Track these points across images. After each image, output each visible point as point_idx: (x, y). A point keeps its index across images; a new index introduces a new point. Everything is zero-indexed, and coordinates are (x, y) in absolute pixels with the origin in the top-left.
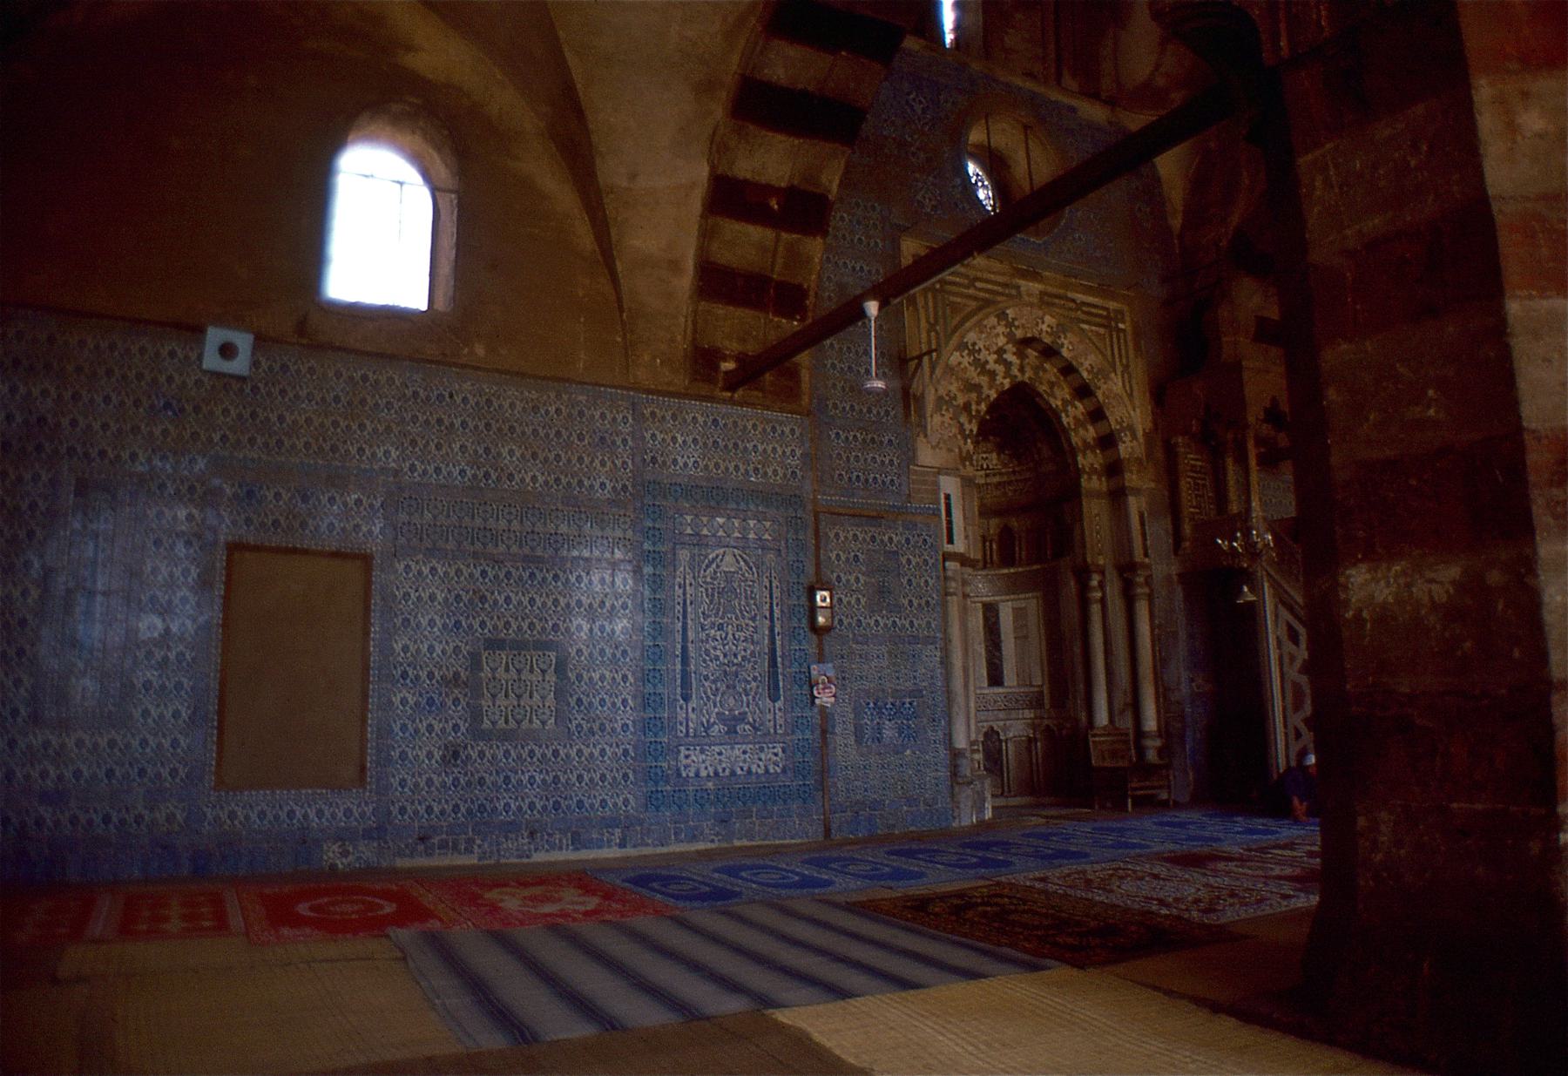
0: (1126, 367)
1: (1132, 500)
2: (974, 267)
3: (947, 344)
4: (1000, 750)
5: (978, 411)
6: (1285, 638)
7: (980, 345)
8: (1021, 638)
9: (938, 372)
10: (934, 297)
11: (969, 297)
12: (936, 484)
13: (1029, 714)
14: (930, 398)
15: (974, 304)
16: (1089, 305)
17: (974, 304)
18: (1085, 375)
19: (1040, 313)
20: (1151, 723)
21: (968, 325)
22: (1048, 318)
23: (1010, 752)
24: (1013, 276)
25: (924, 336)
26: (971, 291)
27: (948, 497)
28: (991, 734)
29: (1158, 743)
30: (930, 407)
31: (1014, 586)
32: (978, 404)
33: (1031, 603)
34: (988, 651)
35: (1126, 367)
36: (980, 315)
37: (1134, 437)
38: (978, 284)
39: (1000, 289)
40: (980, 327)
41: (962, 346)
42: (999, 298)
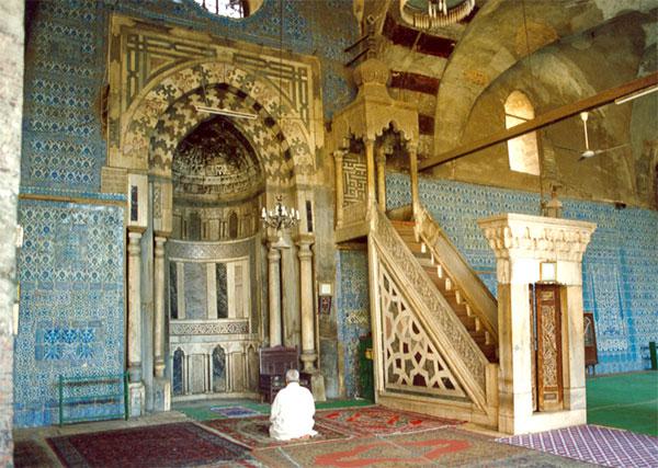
0: (305, 106)
1: (300, 193)
2: (175, 36)
3: (144, 86)
4: (224, 361)
5: (179, 133)
6: (382, 287)
7: (174, 87)
8: (238, 286)
9: (136, 103)
10: (137, 55)
11: (170, 55)
12: (125, 180)
13: (241, 337)
14: (125, 123)
15: (173, 60)
16: (274, 63)
17: (173, 60)
18: (269, 109)
19: (233, 68)
20: (309, 345)
21: (165, 73)
22: (238, 72)
23: (230, 362)
24: (211, 43)
25: (125, 81)
26: (172, 51)
27: (135, 189)
28: (218, 350)
29: (313, 358)
30: (124, 129)
31: (235, 252)
32: (180, 127)
33: (245, 264)
34: (218, 295)
35: (305, 106)
36: (179, 67)
37: (308, 151)
38: (178, 47)
39: (199, 51)
40: (177, 75)
41: (158, 88)
42: (196, 57)
